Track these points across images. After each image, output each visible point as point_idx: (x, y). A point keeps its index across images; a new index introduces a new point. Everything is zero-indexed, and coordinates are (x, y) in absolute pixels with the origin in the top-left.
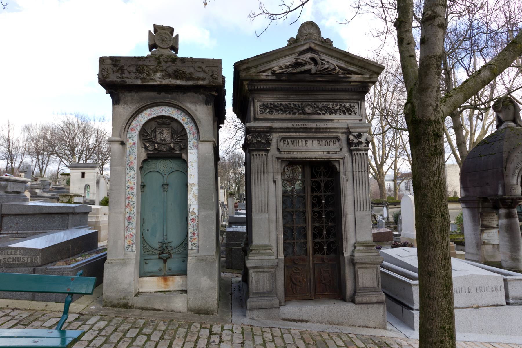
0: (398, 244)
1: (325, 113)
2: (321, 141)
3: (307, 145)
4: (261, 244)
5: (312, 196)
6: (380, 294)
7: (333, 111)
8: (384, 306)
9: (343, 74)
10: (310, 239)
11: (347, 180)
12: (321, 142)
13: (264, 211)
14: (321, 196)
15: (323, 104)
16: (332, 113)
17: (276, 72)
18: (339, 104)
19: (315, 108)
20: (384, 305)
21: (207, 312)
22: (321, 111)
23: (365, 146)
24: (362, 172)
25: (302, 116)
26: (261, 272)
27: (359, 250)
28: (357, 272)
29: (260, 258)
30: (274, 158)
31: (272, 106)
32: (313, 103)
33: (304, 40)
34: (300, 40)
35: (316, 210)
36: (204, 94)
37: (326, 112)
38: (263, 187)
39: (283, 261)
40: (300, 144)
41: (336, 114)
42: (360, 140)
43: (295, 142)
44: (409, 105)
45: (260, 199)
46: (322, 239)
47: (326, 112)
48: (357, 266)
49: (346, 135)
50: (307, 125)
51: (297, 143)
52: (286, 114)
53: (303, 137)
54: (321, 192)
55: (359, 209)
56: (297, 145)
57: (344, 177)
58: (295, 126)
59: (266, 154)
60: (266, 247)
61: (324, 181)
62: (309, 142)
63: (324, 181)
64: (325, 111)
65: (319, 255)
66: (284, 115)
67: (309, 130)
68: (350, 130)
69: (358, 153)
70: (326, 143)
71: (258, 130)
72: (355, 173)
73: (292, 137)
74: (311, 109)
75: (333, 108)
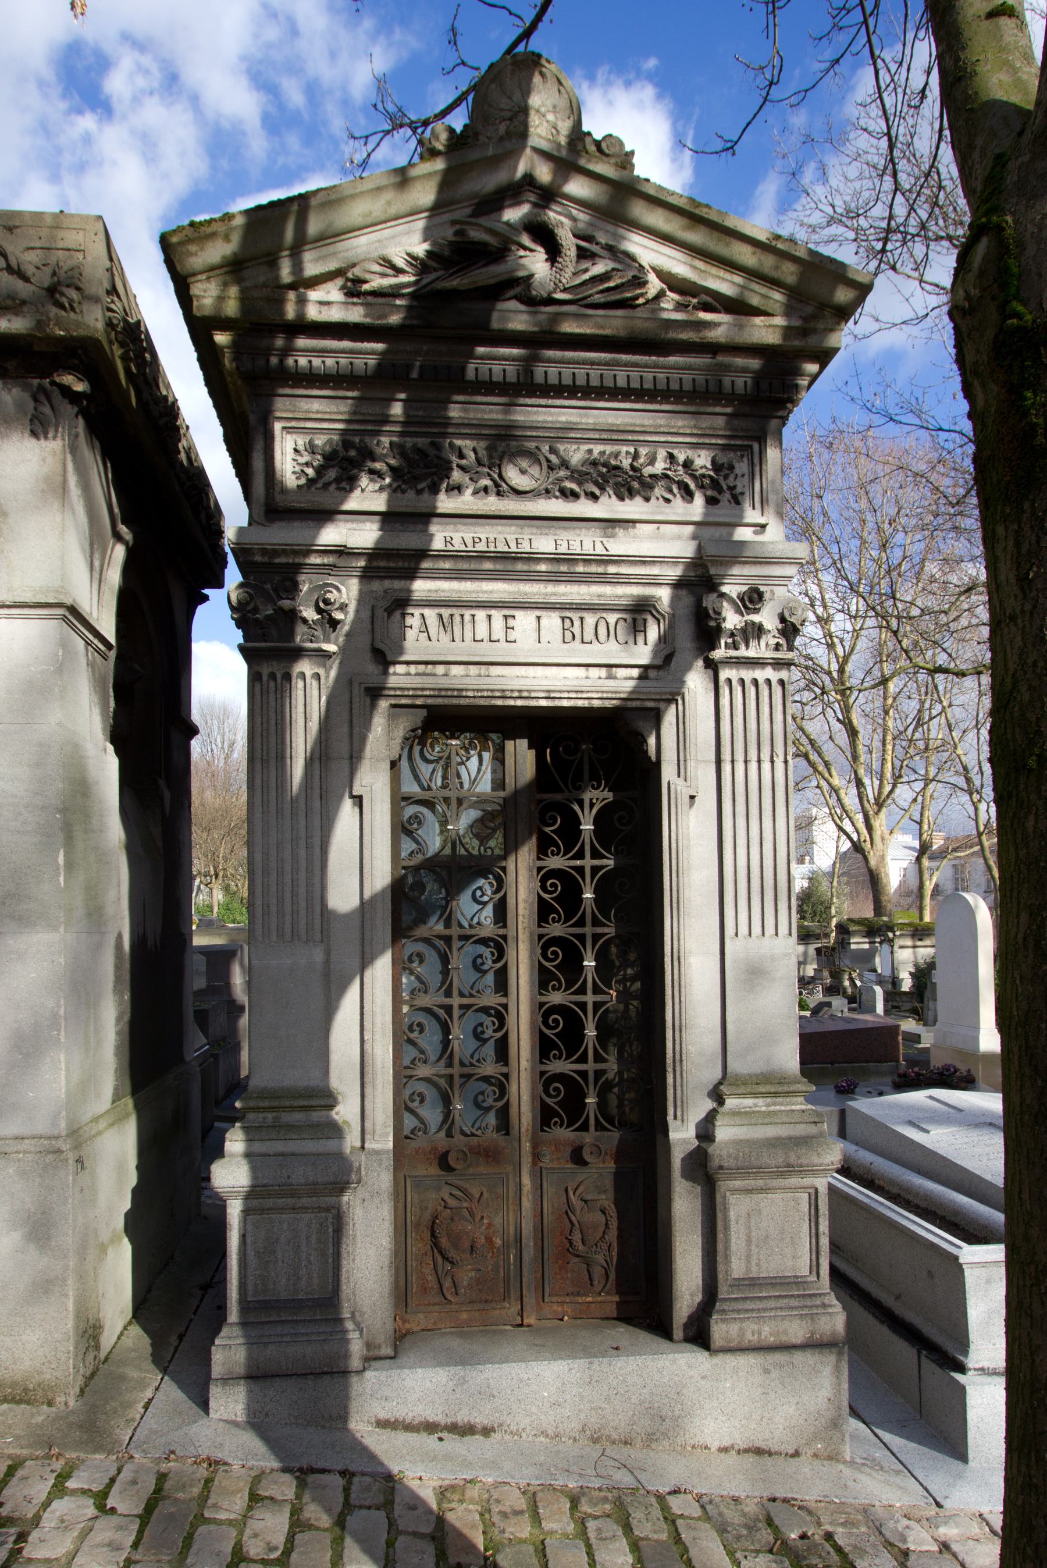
0: (918, 1074)
1: (597, 492)
2: (575, 616)
3: (512, 636)
4: (287, 1082)
5: (540, 869)
6: (824, 1306)
7: (636, 485)
8: (839, 1361)
9: (680, 307)
10: (525, 1064)
11: (692, 797)
12: (577, 623)
13: (303, 932)
14: (580, 870)
15: (590, 451)
16: (631, 493)
17: (366, 287)
18: (662, 454)
19: (551, 468)
20: (840, 1354)
21: (26, 1390)
22: (580, 484)
23: (777, 647)
24: (759, 761)
25: (492, 504)
26: (281, 1210)
27: (735, 1113)
28: (726, 1210)
29: (279, 1146)
30: (356, 691)
31: (353, 453)
32: (545, 448)
33: (501, 139)
34: (482, 139)
35: (557, 933)
36: (26, 387)
37: (602, 489)
38: (303, 823)
39: (389, 1161)
40: (482, 631)
41: (647, 499)
42: (756, 618)
43: (457, 619)
44: (982, 247)
45: (288, 879)
46: (577, 1061)
47: (602, 489)
48: (724, 1186)
49: (692, 593)
50: (513, 545)
51: (468, 627)
52: (419, 492)
53: (495, 597)
54: (580, 855)
55: (743, 929)
56: (469, 635)
57: (678, 784)
58: (458, 545)
59: (321, 672)
60: (311, 1097)
61: (592, 805)
62: (524, 620)
63: (592, 805)
64: (596, 483)
65: (563, 1134)
66: (411, 494)
67: (520, 566)
68: (712, 571)
69: (748, 675)
70: (602, 631)
71: (282, 560)
72: (727, 768)
73: (442, 596)
74: (535, 471)
75: (633, 468)
